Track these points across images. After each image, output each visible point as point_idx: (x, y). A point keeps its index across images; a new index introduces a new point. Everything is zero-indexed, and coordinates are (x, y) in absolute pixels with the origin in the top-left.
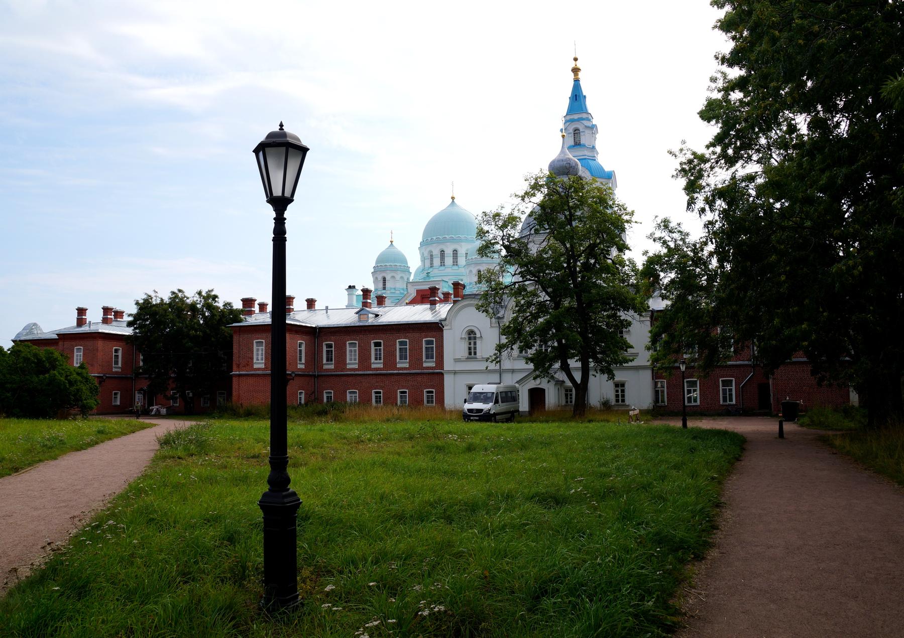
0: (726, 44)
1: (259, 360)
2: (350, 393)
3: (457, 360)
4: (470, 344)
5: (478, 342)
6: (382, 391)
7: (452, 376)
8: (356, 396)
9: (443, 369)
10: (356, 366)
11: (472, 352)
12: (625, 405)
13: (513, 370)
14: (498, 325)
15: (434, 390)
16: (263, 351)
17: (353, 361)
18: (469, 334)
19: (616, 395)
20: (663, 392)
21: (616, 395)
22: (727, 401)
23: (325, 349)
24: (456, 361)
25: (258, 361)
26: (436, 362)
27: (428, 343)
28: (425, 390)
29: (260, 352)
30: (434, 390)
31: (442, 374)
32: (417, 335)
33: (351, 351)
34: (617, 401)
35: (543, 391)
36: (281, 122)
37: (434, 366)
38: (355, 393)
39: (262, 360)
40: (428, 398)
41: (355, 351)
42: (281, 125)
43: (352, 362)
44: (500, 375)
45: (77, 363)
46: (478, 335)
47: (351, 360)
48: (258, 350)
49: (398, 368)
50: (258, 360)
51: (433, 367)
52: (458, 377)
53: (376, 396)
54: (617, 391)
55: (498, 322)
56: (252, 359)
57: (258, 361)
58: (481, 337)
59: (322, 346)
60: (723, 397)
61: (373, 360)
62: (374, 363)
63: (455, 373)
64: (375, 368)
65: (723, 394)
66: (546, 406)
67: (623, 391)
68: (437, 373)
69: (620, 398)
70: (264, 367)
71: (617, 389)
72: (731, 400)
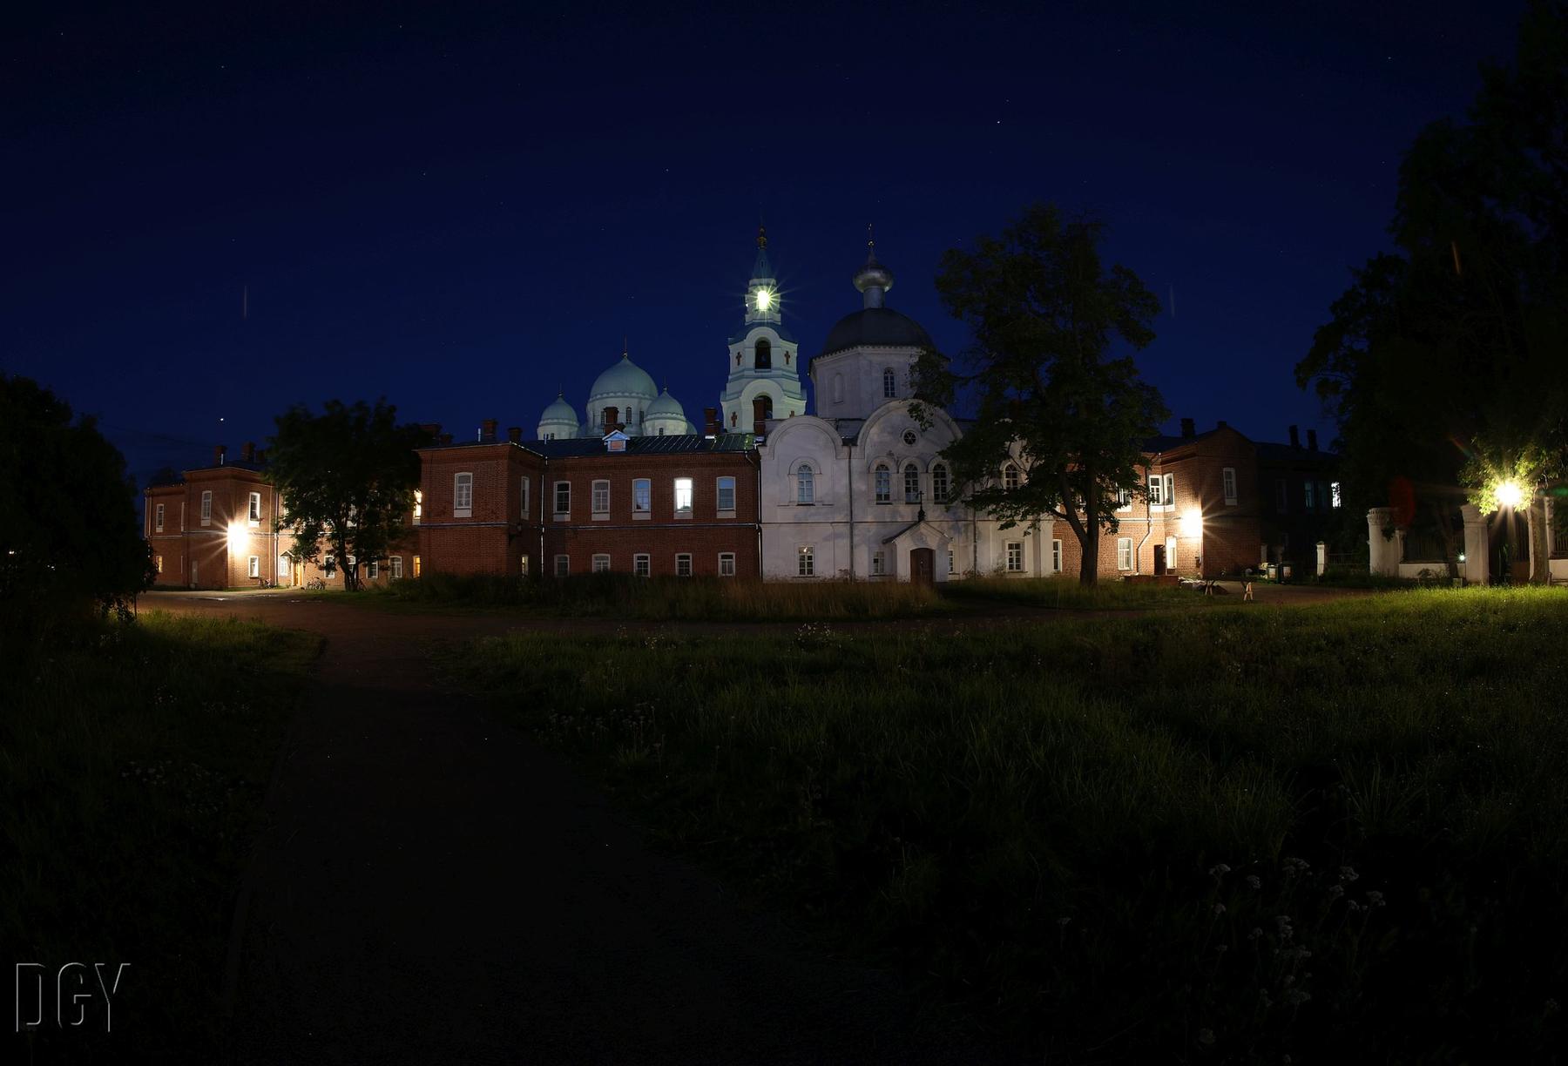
0: (846, 350)
1: (462, 505)
8: (607, 563)
16: (1171, 483)
17: (602, 511)
23: (556, 492)
27: (561, 487)
29: (465, 492)
33: (598, 495)
34: (1011, 567)
36: (787, 352)
38: (731, 557)
39: (467, 504)
41: (605, 495)
45: (254, 498)
48: (461, 489)
50: (460, 504)
53: (680, 563)
56: (452, 503)
59: (552, 487)
66: (1371, 568)
67: (1018, 554)
70: (470, 516)
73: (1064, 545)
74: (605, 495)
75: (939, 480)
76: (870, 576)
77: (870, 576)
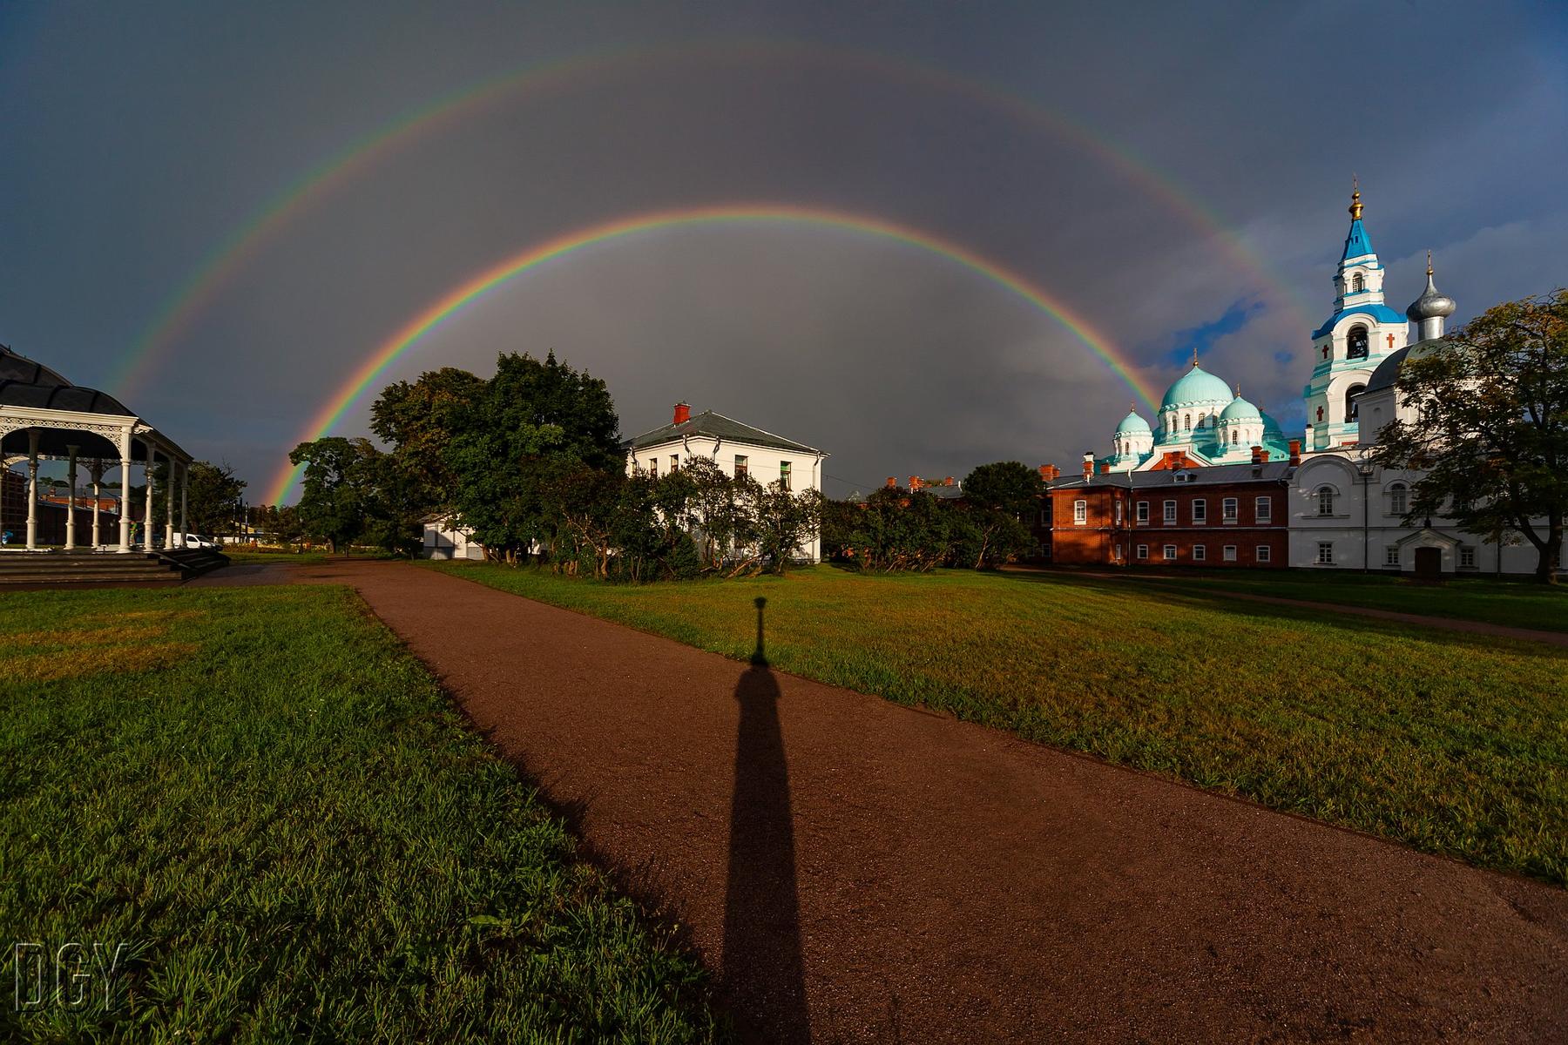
2: (1167, 547)
10: (1175, 523)
11: (1326, 511)
33: (1168, 509)
43: (1229, 520)
46: (1335, 492)
47: (1168, 517)
63: (1303, 530)
74: (1173, 509)
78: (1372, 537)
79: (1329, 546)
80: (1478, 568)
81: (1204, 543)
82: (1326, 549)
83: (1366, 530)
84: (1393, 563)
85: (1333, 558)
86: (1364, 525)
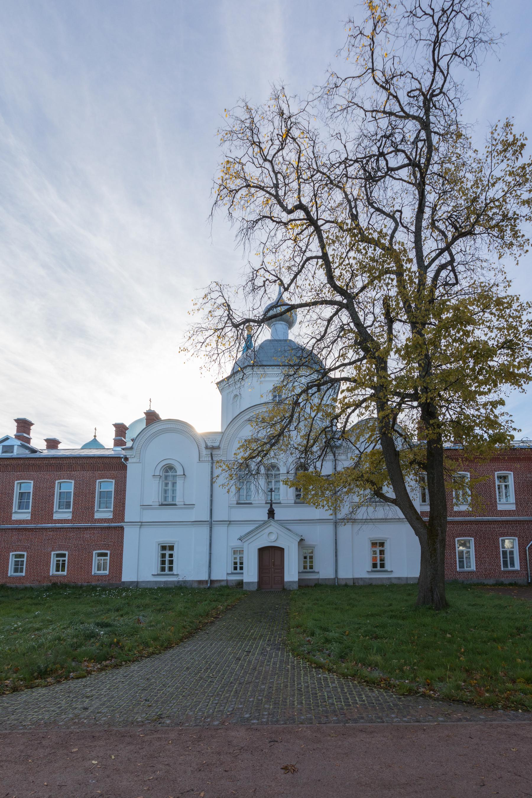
3: (145, 507)
4: (167, 485)
5: (179, 483)
6: (67, 553)
7: (137, 529)
9: (123, 520)
12: (386, 571)
13: (230, 521)
14: (210, 459)
15: (25, 553)
18: (167, 471)
19: (373, 557)
20: (512, 553)
21: (373, 557)
22: (507, 567)
24: (144, 509)
25: (305, 570)
26: (114, 512)
28: (94, 552)
30: (67, 553)
31: (122, 528)
32: (88, 474)
35: (282, 550)
37: (111, 517)
38: (105, 555)
40: (16, 565)
42: (95, 436)
44: (211, 528)
46: (180, 472)
49: (55, 520)
51: (109, 520)
52: (147, 531)
54: (375, 552)
55: (211, 454)
57: (305, 570)
58: (184, 475)
60: (506, 558)
61: (15, 508)
62: (16, 512)
63: (141, 524)
64: (17, 521)
65: (503, 558)
67: (382, 552)
68: (115, 528)
69: (167, 565)
71: (374, 549)
72: (513, 564)
73: (27, 556)
75: (378, 549)
76: (228, 574)
77: (228, 574)
78: (220, 531)
79: (171, 548)
80: (318, 573)
81: (25, 549)
82: (168, 553)
83: (211, 524)
84: (379, 568)
85: (175, 565)
86: (209, 519)
